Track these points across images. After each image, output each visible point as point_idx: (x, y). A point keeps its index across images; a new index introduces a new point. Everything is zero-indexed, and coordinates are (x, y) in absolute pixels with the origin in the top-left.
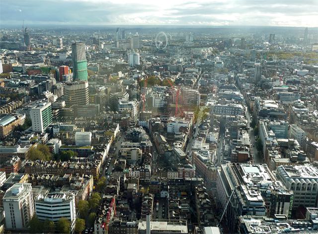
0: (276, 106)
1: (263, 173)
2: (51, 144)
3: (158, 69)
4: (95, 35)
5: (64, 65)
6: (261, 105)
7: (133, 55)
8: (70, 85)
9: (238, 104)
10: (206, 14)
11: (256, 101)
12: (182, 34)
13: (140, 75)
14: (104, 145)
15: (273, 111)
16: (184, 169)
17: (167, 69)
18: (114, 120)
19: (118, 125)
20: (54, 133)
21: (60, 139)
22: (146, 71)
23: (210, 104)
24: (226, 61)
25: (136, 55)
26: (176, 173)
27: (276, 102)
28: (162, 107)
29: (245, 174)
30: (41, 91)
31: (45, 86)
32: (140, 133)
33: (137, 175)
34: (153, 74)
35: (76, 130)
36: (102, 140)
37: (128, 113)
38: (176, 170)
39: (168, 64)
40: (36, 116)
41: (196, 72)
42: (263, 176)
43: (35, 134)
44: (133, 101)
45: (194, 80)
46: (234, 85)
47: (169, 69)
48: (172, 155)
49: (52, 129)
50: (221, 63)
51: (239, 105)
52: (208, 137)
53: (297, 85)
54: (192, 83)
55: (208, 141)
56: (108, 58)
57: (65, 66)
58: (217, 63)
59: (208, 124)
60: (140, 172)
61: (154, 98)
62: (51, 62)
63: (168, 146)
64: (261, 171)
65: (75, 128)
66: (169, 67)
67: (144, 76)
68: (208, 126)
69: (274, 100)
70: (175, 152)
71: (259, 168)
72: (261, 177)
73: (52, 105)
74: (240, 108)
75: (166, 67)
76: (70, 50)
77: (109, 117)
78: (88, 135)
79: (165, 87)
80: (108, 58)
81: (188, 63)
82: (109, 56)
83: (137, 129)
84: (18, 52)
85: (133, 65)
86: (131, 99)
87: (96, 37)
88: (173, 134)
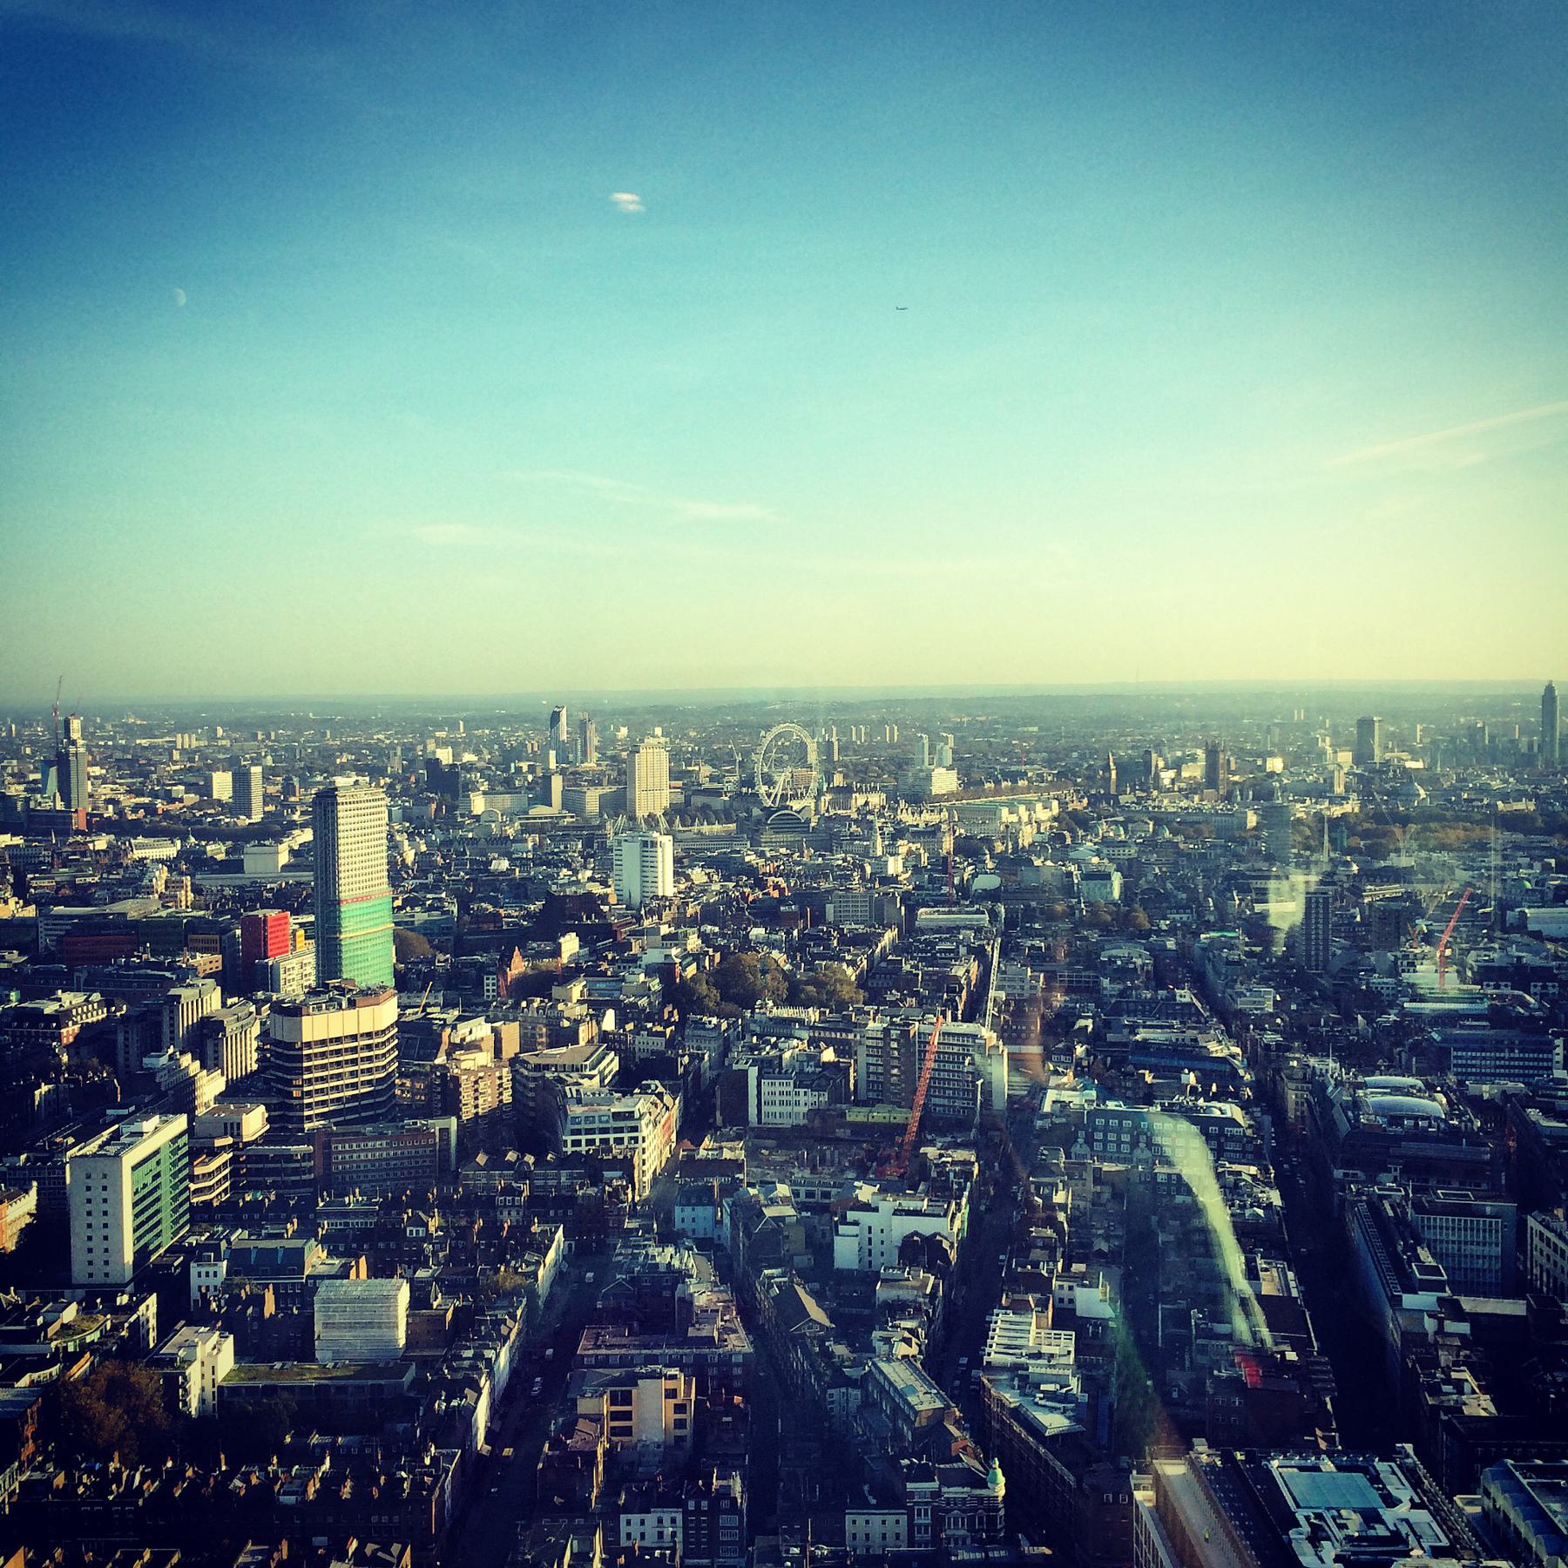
0: (1436, 1105)
1: (1403, 1510)
2: (171, 1360)
3: (768, 914)
4: (442, 743)
5: (266, 905)
6: (1345, 1108)
7: (637, 846)
8: (296, 1011)
9: (1216, 1097)
10: (1456, 1011)
11: (1315, 1084)
12: (893, 734)
13: (674, 951)
14: (478, 1356)
15: (1419, 1135)
16: (936, 1494)
17: (819, 918)
18: (539, 1205)
19: (560, 1234)
20: (195, 1294)
21: (227, 1328)
22: (708, 928)
23: (1064, 1105)
24: (1130, 869)
25: (654, 844)
26: (890, 1519)
27: (1426, 1083)
28: (802, 1122)
29: (1300, 1516)
30: (133, 1050)
31: (159, 1024)
32: (680, 1276)
33: (667, 1537)
34: (747, 945)
35: (322, 1269)
36: (466, 1322)
37: (614, 1164)
38: (892, 1499)
39: (824, 885)
40: (98, 1220)
41: (978, 930)
42: (1404, 1529)
43: (88, 1309)
44: (645, 1090)
45: (965, 970)
46: (1185, 995)
47: (830, 917)
48: (868, 1404)
49: (185, 1267)
50: (1108, 877)
51: (1227, 1107)
52: (1065, 1294)
53: (1536, 987)
54: (953, 986)
55: (1065, 1318)
56: (504, 864)
57: (272, 913)
58: (1088, 877)
59: (1061, 1217)
60: (686, 1513)
61: (753, 1072)
62: (197, 890)
63: (840, 1350)
64: (1391, 1501)
65: (316, 1258)
66: (830, 908)
67: (697, 957)
68: (1057, 1227)
69: (1419, 1074)
70: (882, 1390)
71: (1375, 1479)
72: (1396, 1538)
73: (190, 1131)
74: (1232, 1122)
75: (810, 902)
76: (303, 826)
77: (509, 1190)
78: (389, 1300)
79: (813, 1015)
80: (504, 864)
81: (931, 880)
82: (508, 855)
83: (665, 1256)
84: (18, 840)
85: (636, 899)
86: (626, 1082)
87: (445, 756)
88: (867, 1277)
